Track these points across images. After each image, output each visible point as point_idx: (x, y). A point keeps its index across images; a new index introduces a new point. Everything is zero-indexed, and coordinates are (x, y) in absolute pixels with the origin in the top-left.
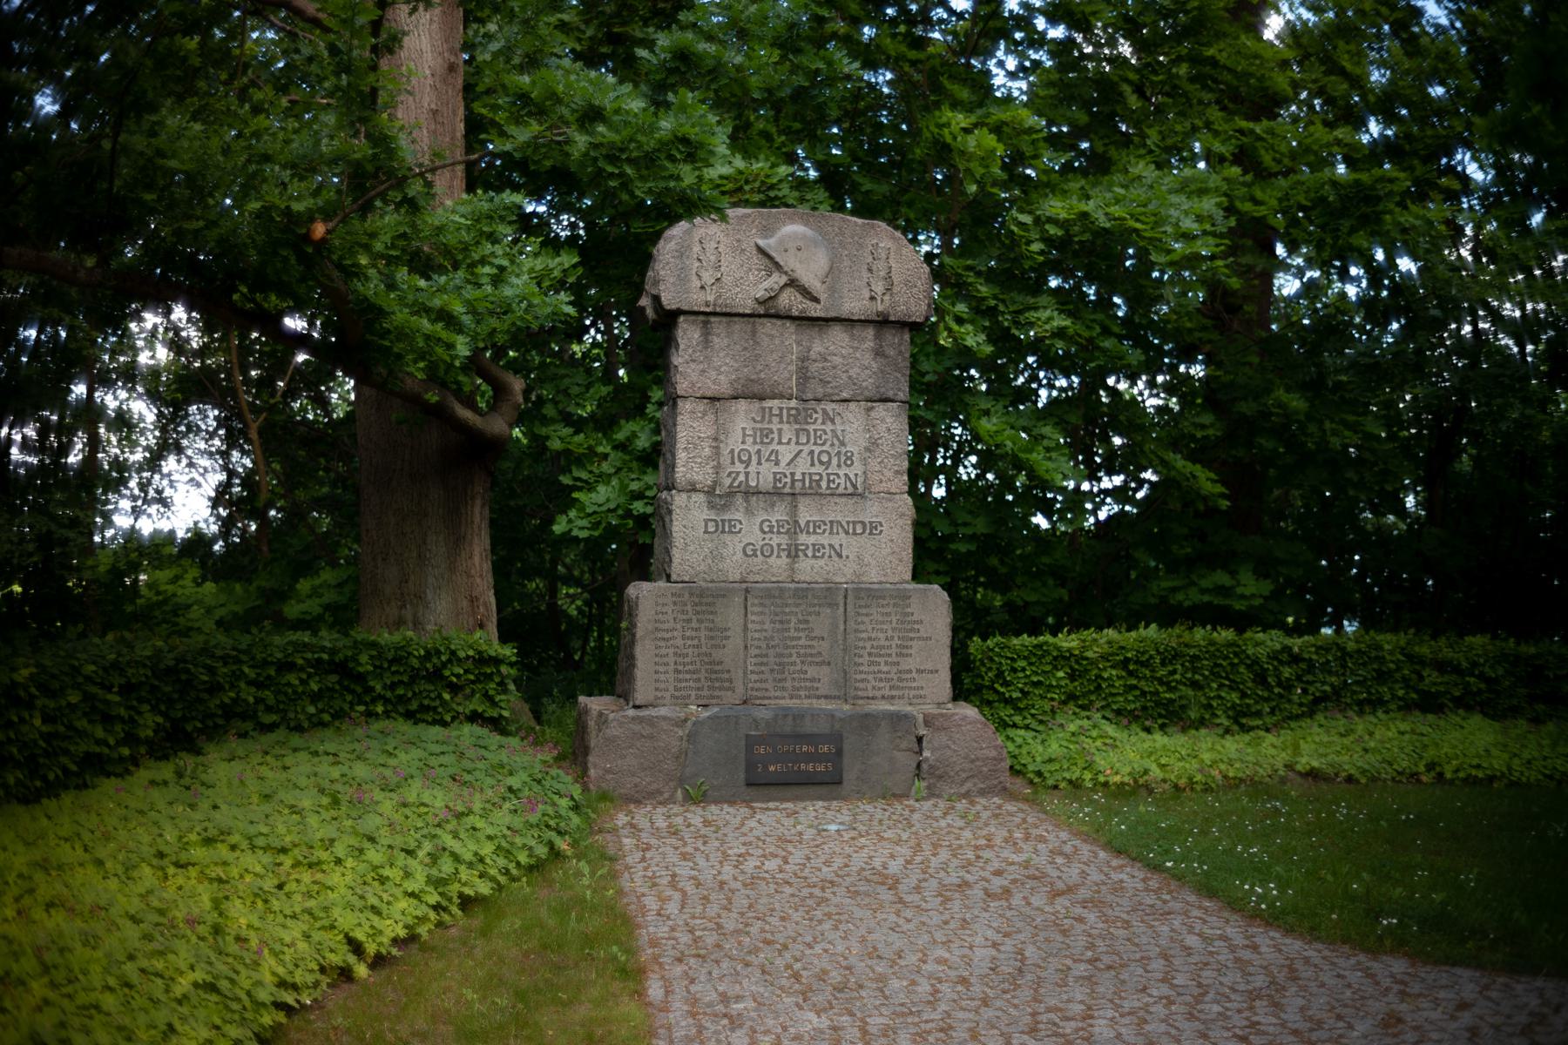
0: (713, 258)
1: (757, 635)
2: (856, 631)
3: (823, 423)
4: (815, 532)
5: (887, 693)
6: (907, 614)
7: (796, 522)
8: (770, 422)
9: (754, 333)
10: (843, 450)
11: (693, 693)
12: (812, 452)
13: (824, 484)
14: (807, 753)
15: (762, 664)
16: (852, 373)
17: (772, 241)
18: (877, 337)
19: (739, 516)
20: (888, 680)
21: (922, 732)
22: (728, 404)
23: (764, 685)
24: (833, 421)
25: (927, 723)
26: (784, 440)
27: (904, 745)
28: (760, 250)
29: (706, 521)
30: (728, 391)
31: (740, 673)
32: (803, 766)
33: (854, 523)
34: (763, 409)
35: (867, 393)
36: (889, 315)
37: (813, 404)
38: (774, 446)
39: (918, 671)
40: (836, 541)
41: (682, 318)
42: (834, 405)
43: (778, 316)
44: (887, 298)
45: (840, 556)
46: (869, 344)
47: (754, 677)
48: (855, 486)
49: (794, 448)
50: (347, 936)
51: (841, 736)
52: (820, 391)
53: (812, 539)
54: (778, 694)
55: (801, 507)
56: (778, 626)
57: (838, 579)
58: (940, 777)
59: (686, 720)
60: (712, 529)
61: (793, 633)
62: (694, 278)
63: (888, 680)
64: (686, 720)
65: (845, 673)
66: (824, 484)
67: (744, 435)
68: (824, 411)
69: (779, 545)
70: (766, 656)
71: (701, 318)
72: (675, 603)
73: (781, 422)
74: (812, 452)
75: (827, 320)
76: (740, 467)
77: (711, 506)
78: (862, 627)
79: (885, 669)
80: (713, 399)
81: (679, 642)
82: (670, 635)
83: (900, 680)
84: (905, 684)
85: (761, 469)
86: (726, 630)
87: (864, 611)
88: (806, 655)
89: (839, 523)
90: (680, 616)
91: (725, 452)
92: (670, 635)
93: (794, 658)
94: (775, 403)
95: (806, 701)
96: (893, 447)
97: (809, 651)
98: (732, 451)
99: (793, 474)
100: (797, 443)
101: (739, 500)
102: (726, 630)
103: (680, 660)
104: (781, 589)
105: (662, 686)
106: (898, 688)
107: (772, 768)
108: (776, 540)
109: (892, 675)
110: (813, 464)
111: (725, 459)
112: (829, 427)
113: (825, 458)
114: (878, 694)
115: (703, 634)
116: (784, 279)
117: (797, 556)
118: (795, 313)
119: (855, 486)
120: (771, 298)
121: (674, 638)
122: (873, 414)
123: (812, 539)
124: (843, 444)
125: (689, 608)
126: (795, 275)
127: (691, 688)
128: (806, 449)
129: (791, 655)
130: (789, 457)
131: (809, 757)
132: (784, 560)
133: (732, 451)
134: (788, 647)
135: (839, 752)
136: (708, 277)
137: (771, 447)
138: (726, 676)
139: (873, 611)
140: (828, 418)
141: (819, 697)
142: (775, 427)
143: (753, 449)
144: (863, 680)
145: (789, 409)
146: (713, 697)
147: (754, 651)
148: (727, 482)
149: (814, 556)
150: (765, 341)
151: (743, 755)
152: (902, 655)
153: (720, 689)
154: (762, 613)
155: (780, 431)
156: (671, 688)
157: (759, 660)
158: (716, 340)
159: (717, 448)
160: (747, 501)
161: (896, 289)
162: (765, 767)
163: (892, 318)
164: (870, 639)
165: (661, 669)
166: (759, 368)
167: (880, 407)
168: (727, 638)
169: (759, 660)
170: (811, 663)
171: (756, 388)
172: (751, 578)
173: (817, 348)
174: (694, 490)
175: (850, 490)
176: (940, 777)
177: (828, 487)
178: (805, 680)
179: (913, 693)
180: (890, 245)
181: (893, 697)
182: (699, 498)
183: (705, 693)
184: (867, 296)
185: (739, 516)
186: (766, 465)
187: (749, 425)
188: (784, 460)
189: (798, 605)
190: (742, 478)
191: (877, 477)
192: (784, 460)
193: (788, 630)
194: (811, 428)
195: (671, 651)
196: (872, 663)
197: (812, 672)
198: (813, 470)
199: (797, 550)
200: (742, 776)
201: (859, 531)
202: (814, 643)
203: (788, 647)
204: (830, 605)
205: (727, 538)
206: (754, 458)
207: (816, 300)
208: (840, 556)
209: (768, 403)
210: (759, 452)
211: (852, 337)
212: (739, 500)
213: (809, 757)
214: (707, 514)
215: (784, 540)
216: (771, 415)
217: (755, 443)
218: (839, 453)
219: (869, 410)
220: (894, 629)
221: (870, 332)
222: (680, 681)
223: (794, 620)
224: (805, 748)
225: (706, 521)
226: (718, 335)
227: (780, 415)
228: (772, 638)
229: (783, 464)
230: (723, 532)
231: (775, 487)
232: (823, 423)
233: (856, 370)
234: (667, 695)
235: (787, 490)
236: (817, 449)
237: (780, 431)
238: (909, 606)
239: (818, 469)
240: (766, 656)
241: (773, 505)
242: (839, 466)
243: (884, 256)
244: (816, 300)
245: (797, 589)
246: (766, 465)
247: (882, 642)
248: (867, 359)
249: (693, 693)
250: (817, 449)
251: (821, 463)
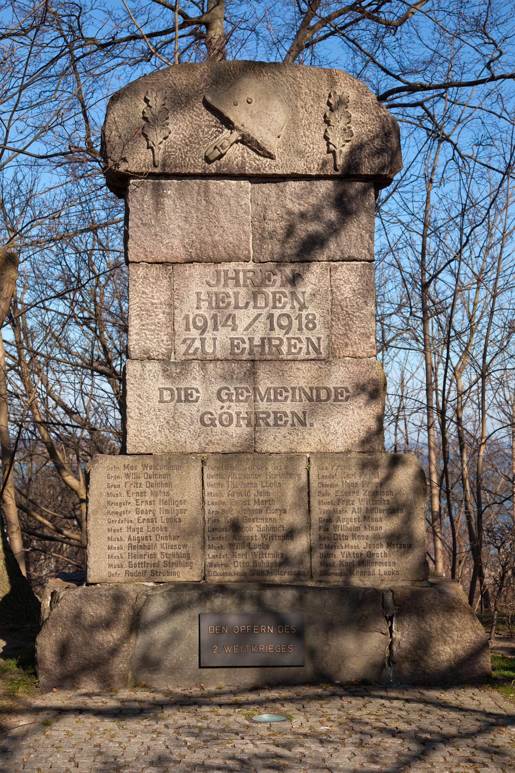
4: (276, 400)
29: (161, 390)
30: (181, 254)
33: (318, 389)
48: (317, 350)
49: (252, 312)
50: (157, 211)
60: (167, 398)
67: (199, 300)
69: (238, 414)
72: (127, 476)
73: (237, 284)
77: (167, 374)
81: (134, 516)
82: (123, 509)
90: (133, 489)
91: (179, 319)
92: (123, 509)
99: (251, 340)
100: (255, 307)
101: (196, 366)
111: (180, 326)
113: (285, 322)
115: (158, 507)
116: (236, 135)
118: (249, 171)
119: (317, 350)
121: (127, 512)
123: (274, 406)
125: (143, 481)
130: (246, 322)
133: (187, 317)
137: (227, 312)
142: (230, 291)
145: (245, 272)
148: (182, 349)
149: (276, 425)
155: (236, 294)
156: (126, 564)
160: (203, 368)
165: (115, 544)
174: (150, 359)
175: (313, 355)
177: (289, 352)
182: (153, 367)
187: (204, 290)
190: (197, 344)
199: (257, 418)
206: (295, 323)
207: (271, 157)
212: (196, 366)
214: (162, 382)
217: (210, 307)
225: (161, 390)
229: (240, 329)
230: (179, 401)
237: (236, 294)
239: (278, 333)
242: (300, 329)
244: (271, 157)
250: (277, 313)
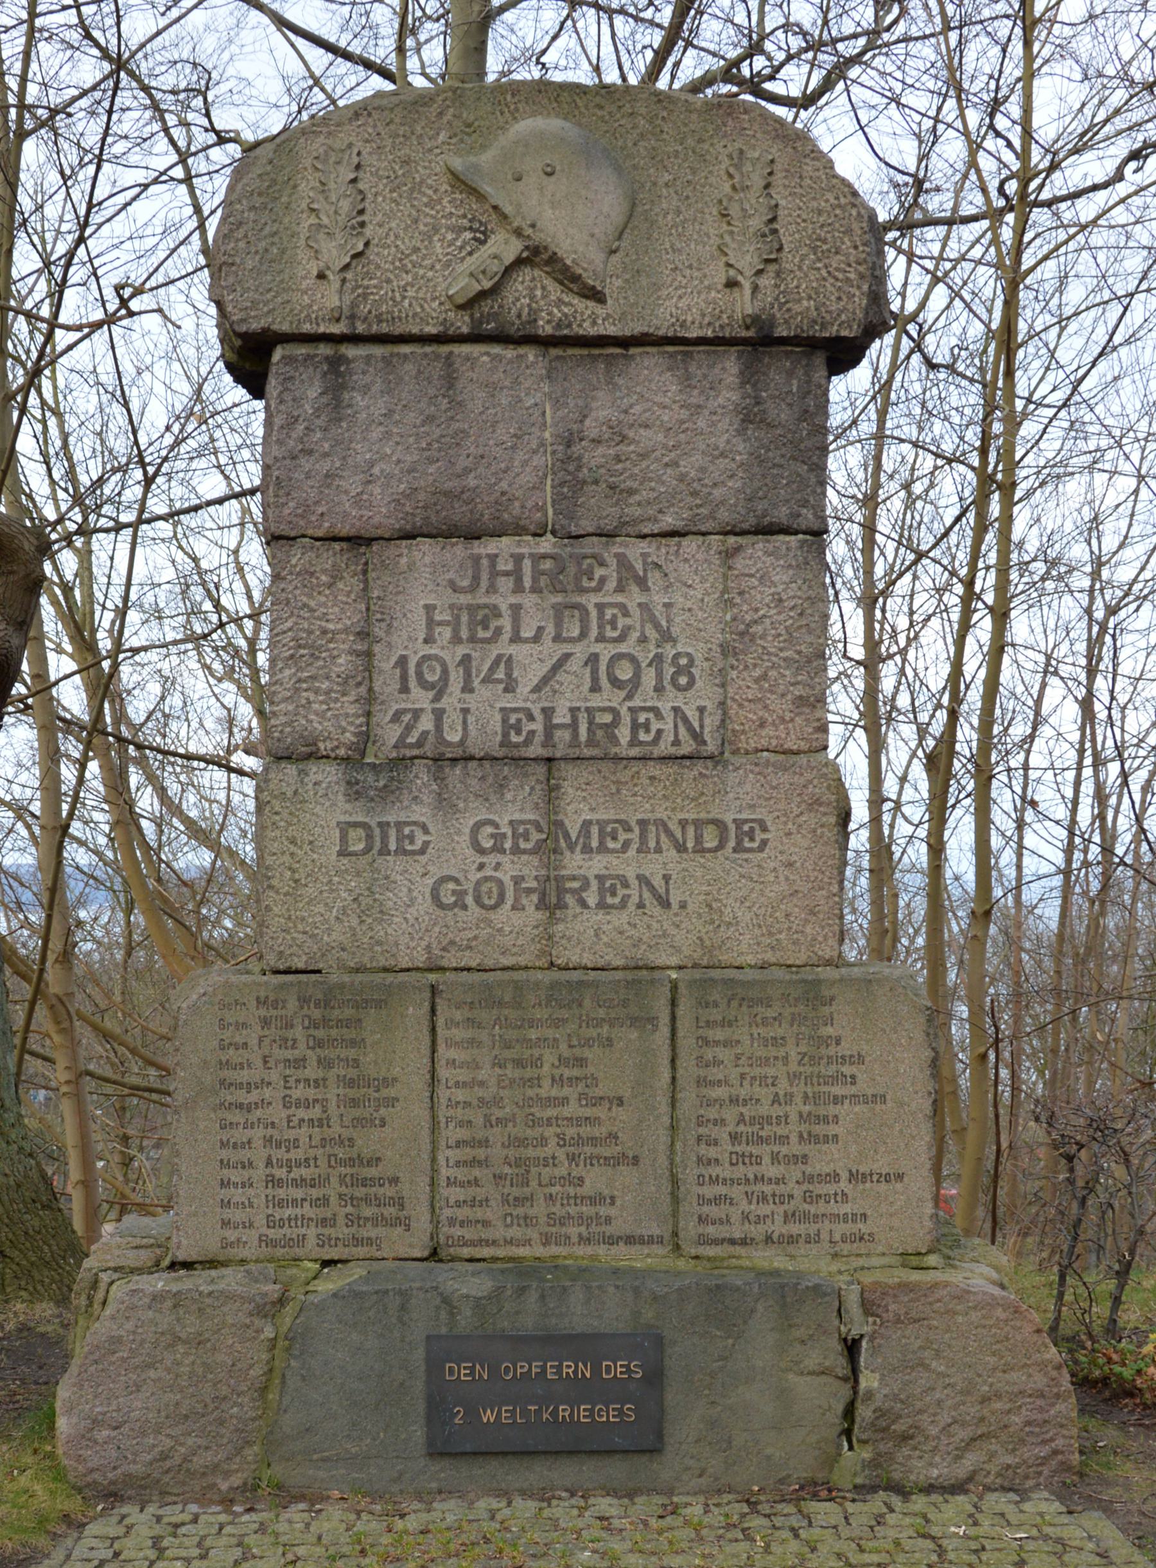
0: (345, 205)
1: (460, 1095)
2: (701, 1082)
3: (620, 589)
4: (602, 849)
5: (778, 1228)
6: (825, 1041)
7: (560, 824)
8: (492, 589)
9: (450, 380)
10: (669, 651)
11: (312, 1232)
12: (593, 659)
13: (624, 734)
14: (575, 1380)
15: (474, 1162)
16: (685, 466)
17: (486, 158)
18: (749, 377)
19: (420, 813)
20: (781, 1199)
21: (858, 1325)
22: (392, 550)
23: (479, 1213)
24: (642, 583)
25: (868, 1308)
26: (527, 633)
27: (813, 1359)
28: (460, 183)
31: (423, 1183)
32: (564, 1411)
33: (698, 824)
34: (476, 559)
35: (724, 515)
36: (772, 322)
37: (592, 545)
38: (503, 647)
39: (853, 1176)
40: (653, 868)
41: (278, 354)
42: (644, 546)
43: (501, 338)
44: (766, 281)
45: (665, 904)
46: (729, 396)
47: (456, 1194)
48: (697, 737)
49: (550, 651)
51: (659, 1342)
52: (609, 516)
53: (597, 865)
54: (515, 1232)
55: (569, 790)
56: (510, 1072)
57: (662, 959)
58: (905, 1438)
59: (282, 1301)
61: (546, 1090)
62: (302, 255)
63: (781, 1199)
64: (282, 1301)
65: (675, 1181)
66: (624, 734)
67: (431, 623)
68: (623, 562)
69: (517, 880)
70: (485, 1143)
71: (324, 350)
73: (519, 588)
74: (593, 659)
75: (625, 342)
76: (420, 698)
77: (355, 791)
78: (716, 1073)
79: (773, 1171)
80: (357, 541)
81: (278, 1113)
82: (254, 1096)
83: (809, 1197)
84: (821, 1208)
85: (472, 701)
86: (387, 1082)
87: (719, 1034)
88: (579, 1141)
89: (662, 824)
90: (279, 1053)
91: (385, 664)
93: (551, 1148)
94: (504, 545)
95: (580, 1251)
96: (791, 640)
97: (586, 1131)
98: (402, 661)
99: (548, 712)
100: (557, 638)
101: (421, 775)
102: (387, 1082)
103: (280, 1154)
104: (518, 986)
105: (238, 1215)
106: (806, 1217)
107: (488, 1416)
108: (509, 869)
109: (791, 1187)
110: (595, 688)
111: (386, 681)
112: (634, 597)
113: (625, 673)
114: (757, 1231)
117: (561, 905)
119: (697, 737)
120: (482, 295)
121: (263, 1103)
122: (739, 563)
124: (667, 637)
125: (298, 1032)
126: (538, 237)
127: (306, 1221)
128: (580, 652)
129: (543, 1141)
130: (538, 671)
131: (579, 1390)
132: (532, 915)
133: (402, 661)
134: (535, 1122)
135: (655, 1378)
136: (334, 253)
138: (388, 1191)
139: (741, 1033)
140: (630, 577)
141: (612, 1241)
143: (452, 655)
144: (717, 1200)
146: (357, 1241)
147: (453, 1133)
148: (392, 734)
149: (602, 905)
150: (475, 399)
151: (419, 1386)
152: (814, 1139)
153: (375, 1221)
154: (472, 1042)
155: (516, 609)
156: (260, 1221)
157: (467, 1153)
158: (359, 400)
159: (369, 654)
160: (439, 778)
161: (789, 260)
162: (472, 1414)
163: (781, 331)
164: (734, 1101)
165: (235, 1176)
166: (462, 463)
167: (757, 548)
168: (392, 1102)
169: (467, 1153)
170: (591, 1160)
171: (459, 513)
172: (451, 959)
173: (603, 410)
174: (313, 756)
176: (905, 1438)
177: (634, 742)
178: (579, 1199)
179: (840, 1229)
180: (775, 152)
181: (792, 1240)
182: (326, 774)
183: (342, 1231)
184: (721, 279)
185: (420, 813)
186: (483, 692)
187: (443, 600)
188: (528, 680)
189: (558, 1023)
190: (426, 723)
191: (752, 715)
192: (528, 680)
193: (536, 1082)
194: (591, 601)
195: (258, 1133)
196: (739, 1159)
197: (595, 1180)
198: (596, 701)
199: (561, 891)
200: (418, 1433)
201: (710, 842)
202: (600, 1112)
203: (535, 1122)
204: (635, 1021)
205: (394, 865)
207: (596, 296)
208: (665, 904)
209: (490, 546)
210: (466, 660)
211: (686, 382)
212: (421, 775)
213: (579, 1390)
214: (342, 810)
215: (530, 868)
216: (494, 574)
217: (456, 639)
218: (658, 659)
219: (729, 555)
220: (793, 1077)
221: (730, 366)
222: (281, 1204)
223: (549, 1058)
224: (568, 1368)
225: (345, 828)
226: (366, 390)
227: (517, 574)
228: (497, 1101)
229: (524, 689)
230: (384, 851)
231: (505, 743)
232: (620, 589)
233: (697, 459)
234: (253, 1236)
235: (535, 750)
236: (605, 652)
237: (516, 609)
238: (830, 1021)
239: (609, 697)
240: (485, 1143)
241: (501, 787)
242: (659, 689)
243: (758, 182)
244: (596, 296)
245: (554, 985)
246: (483, 692)
247: (765, 1109)
248: (724, 432)
249: (312, 1232)
250: (605, 652)
251: (615, 683)
